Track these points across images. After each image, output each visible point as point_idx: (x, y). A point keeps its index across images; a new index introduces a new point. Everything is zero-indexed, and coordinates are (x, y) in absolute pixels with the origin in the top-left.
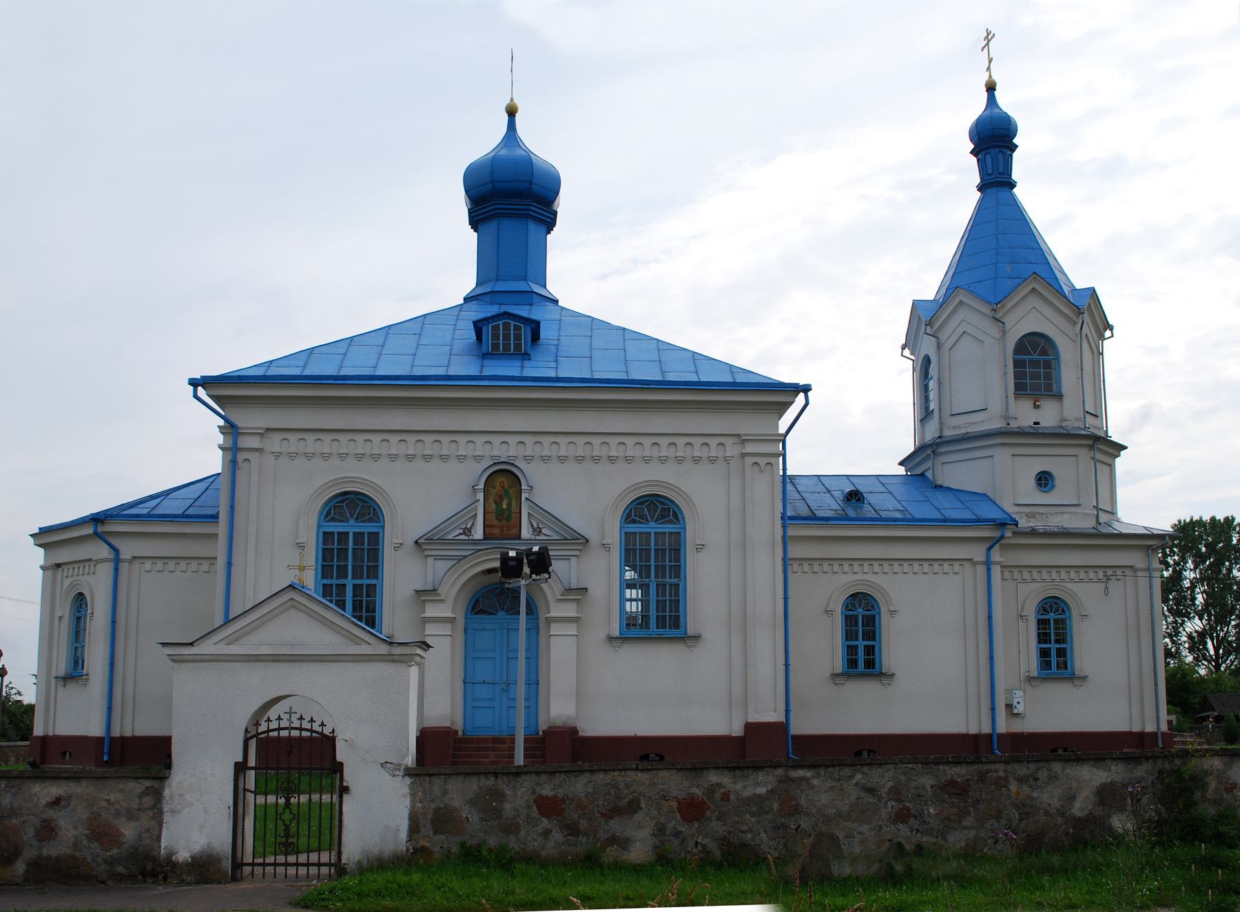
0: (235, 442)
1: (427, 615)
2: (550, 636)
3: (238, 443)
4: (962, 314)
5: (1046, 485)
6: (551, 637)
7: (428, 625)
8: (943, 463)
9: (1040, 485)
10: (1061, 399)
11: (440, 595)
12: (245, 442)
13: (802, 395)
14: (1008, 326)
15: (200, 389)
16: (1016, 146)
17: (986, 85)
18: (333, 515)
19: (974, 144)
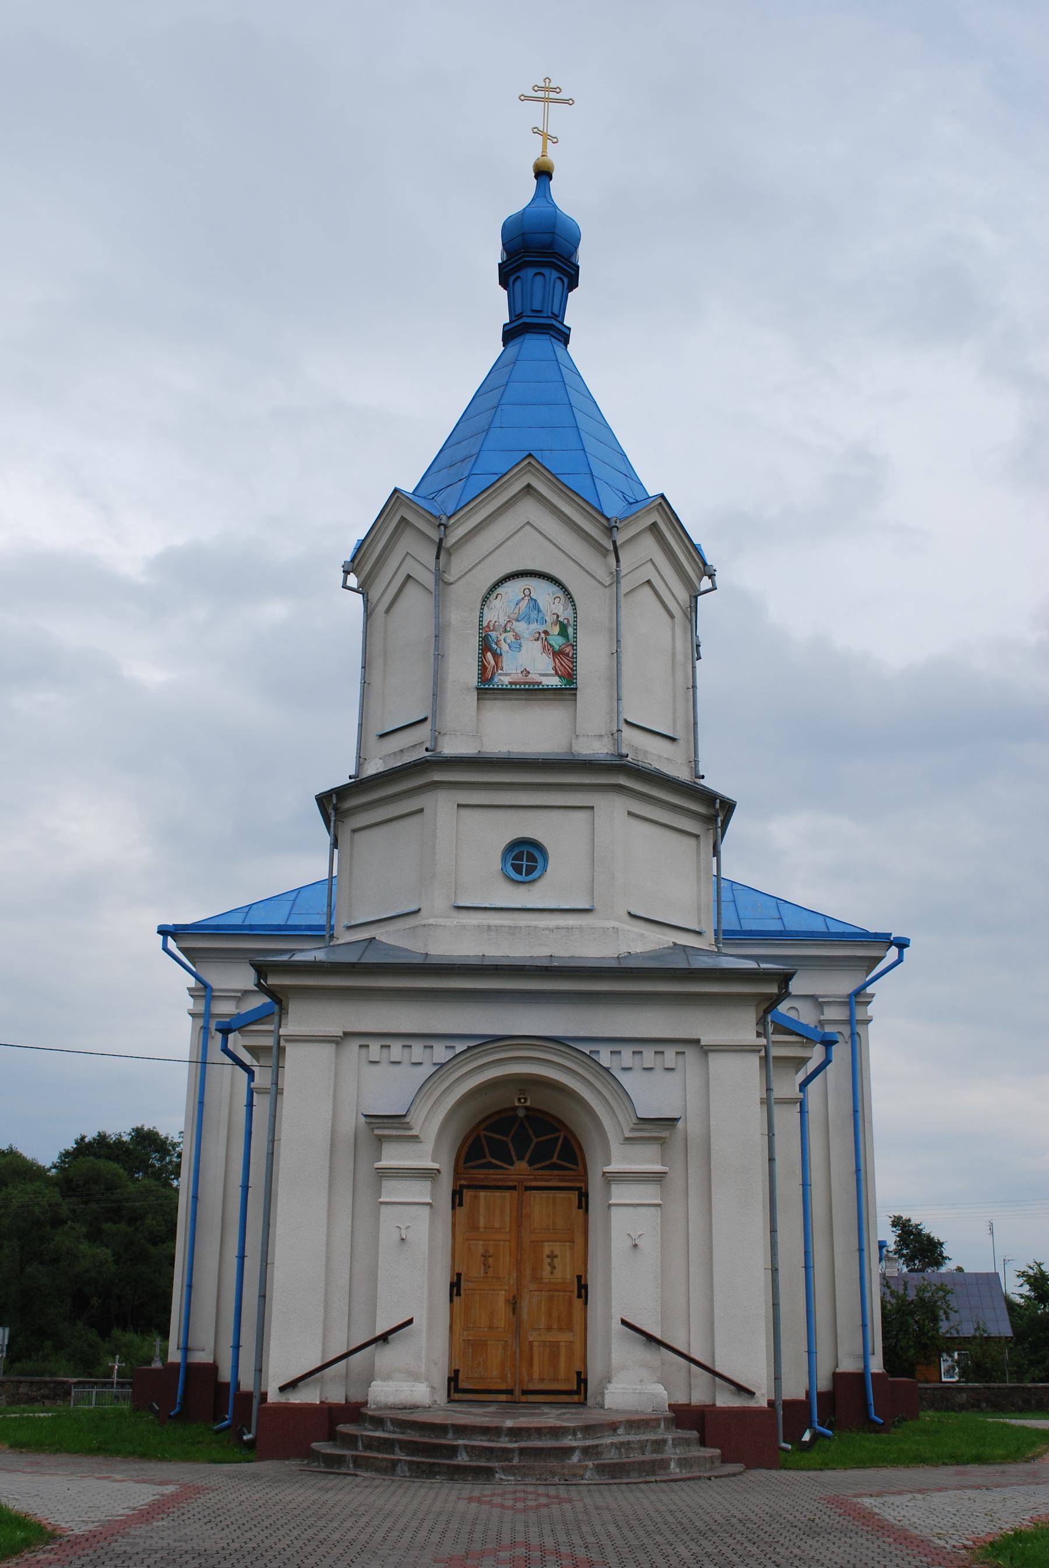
0: (208, 1007)
1: (384, 1163)
2: (610, 1206)
3: (212, 1009)
5: (530, 870)
6: (613, 1208)
7: (387, 1184)
8: (354, 831)
9: (518, 869)
11: (410, 1129)
13: (894, 950)
14: (624, 567)
15: (170, 941)
18: (535, 1140)
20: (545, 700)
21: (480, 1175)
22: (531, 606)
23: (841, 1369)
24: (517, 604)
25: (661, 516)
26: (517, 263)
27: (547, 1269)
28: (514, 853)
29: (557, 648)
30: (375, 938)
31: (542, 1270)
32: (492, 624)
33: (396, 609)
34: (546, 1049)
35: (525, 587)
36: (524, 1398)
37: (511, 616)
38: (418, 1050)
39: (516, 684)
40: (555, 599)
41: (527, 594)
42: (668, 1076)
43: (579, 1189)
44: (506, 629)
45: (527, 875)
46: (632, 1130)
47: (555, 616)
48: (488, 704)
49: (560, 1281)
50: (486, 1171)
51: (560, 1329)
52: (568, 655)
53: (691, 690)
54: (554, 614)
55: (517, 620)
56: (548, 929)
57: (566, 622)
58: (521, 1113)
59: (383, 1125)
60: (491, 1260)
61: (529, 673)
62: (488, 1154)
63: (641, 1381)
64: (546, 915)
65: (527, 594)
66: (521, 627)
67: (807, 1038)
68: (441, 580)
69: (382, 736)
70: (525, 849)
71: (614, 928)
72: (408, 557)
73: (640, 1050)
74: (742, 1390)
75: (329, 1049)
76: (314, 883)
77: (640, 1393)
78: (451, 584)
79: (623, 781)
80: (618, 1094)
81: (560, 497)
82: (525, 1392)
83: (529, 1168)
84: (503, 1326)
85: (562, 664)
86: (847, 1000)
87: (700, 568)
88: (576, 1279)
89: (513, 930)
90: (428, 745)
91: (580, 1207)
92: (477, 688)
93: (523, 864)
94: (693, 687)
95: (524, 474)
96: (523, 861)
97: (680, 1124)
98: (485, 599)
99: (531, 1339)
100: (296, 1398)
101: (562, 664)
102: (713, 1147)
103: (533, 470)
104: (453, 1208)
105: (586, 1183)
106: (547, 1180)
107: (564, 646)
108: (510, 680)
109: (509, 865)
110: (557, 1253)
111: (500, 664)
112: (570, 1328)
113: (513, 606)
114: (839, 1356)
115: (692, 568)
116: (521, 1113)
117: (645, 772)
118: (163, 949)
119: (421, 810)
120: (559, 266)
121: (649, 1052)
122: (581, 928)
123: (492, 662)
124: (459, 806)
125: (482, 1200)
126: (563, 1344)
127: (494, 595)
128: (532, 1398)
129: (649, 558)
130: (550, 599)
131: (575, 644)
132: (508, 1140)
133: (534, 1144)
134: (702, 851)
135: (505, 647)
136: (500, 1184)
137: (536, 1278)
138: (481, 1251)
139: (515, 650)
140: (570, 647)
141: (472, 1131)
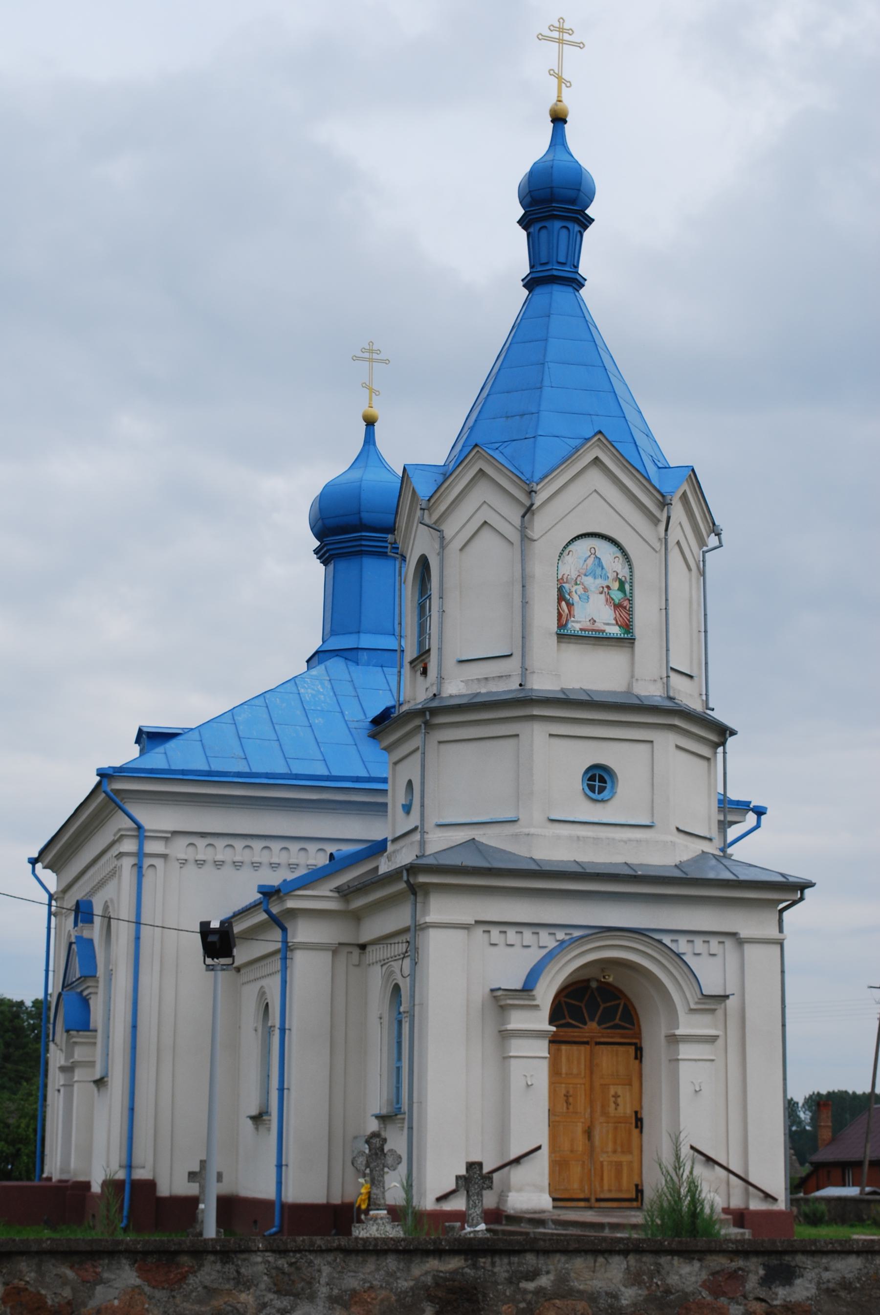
0: (141, 846)
5: (602, 790)
8: (440, 742)
9: (592, 788)
10: (633, 643)
11: (534, 1000)
12: (151, 847)
16: (591, 220)
17: (551, 115)
18: (602, 1006)
19: (524, 208)
20: (608, 645)
22: (596, 564)
24: (585, 561)
25: (690, 487)
27: (613, 1106)
29: (617, 601)
30: (474, 839)
31: (609, 1107)
32: (565, 577)
33: (468, 549)
34: (647, 944)
35: (591, 546)
37: (581, 571)
38: (528, 935)
39: (585, 630)
40: (615, 558)
41: (593, 552)
43: (635, 1044)
44: (576, 582)
47: (615, 574)
48: (564, 646)
49: (622, 1115)
51: (623, 1152)
52: (625, 608)
53: (664, 611)
54: (614, 572)
55: (585, 575)
56: (621, 841)
57: (623, 579)
61: (595, 621)
62: (567, 1017)
64: (618, 829)
65: (593, 552)
66: (588, 581)
68: (525, 538)
71: (671, 842)
72: (485, 506)
74: (768, 1197)
76: (208, 722)
78: (535, 540)
79: (677, 722)
80: (687, 976)
81: (622, 470)
82: (598, 1200)
85: (621, 616)
87: (710, 527)
88: (634, 1114)
91: (636, 1058)
92: (558, 634)
93: (595, 785)
94: (666, 609)
96: (595, 781)
97: (731, 1003)
99: (601, 1159)
101: (621, 616)
105: (640, 1038)
106: (612, 1037)
107: (622, 600)
110: (620, 1093)
111: (572, 612)
112: (630, 1152)
113: (582, 562)
115: (704, 526)
116: (594, 985)
117: (694, 715)
125: (563, 1052)
126: (625, 1163)
127: (567, 551)
131: (631, 599)
132: (582, 1005)
135: (576, 598)
137: (604, 1113)
138: (563, 1092)
140: (627, 601)
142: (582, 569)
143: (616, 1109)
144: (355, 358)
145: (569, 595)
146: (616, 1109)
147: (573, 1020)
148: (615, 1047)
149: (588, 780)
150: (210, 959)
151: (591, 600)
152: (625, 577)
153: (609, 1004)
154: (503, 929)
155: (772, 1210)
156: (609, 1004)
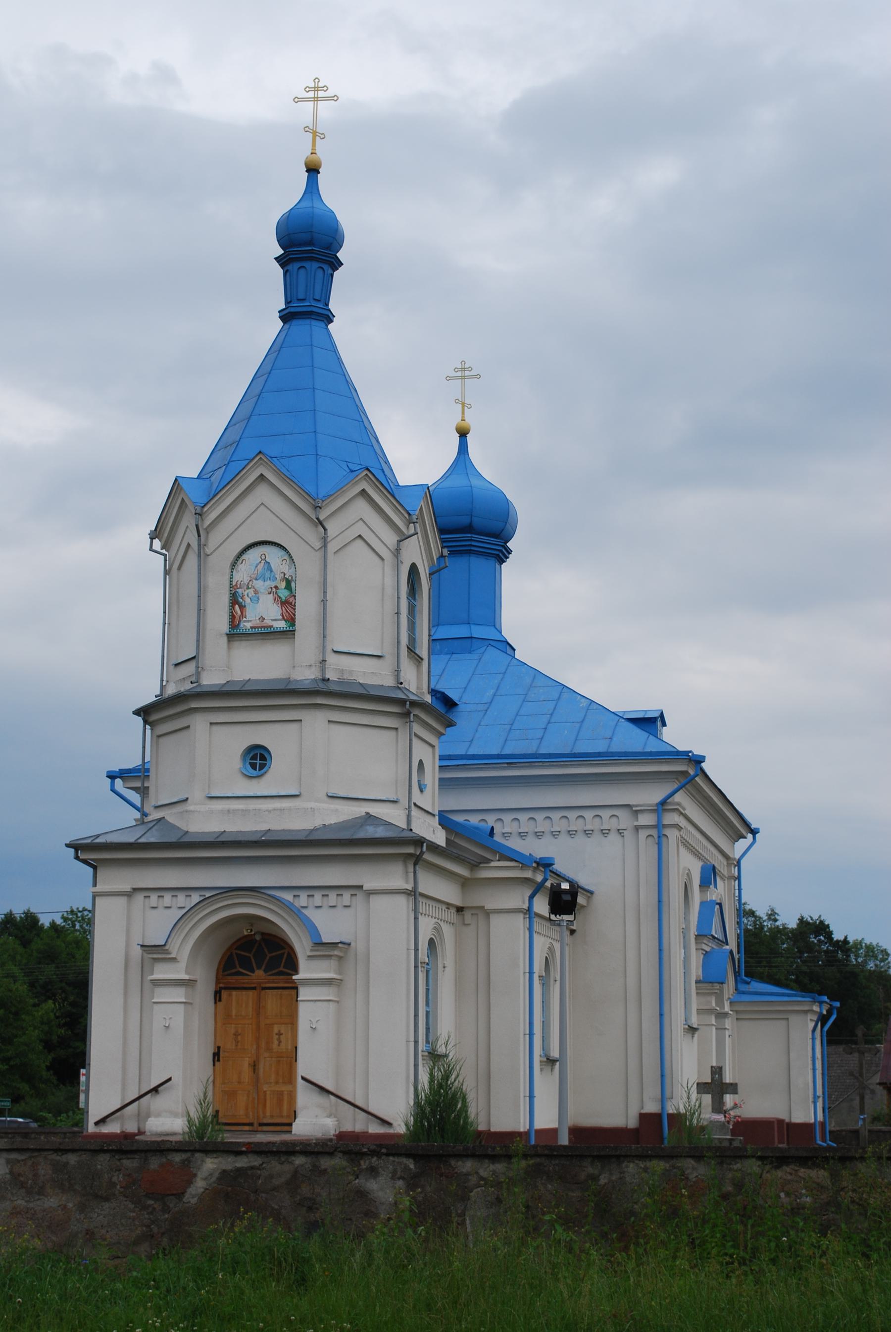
0: (659, 819)
4: (263, 493)
5: (262, 767)
7: (158, 990)
9: (253, 766)
11: (170, 953)
14: (331, 533)
15: (118, 781)
18: (269, 956)
21: (232, 980)
23: (645, 1111)
26: (285, 259)
27: (276, 1042)
28: (251, 755)
29: (284, 599)
31: (273, 1043)
32: (239, 583)
33: (184, 567)
35: (262, 553)
36: (260, 1128)
38: (168, 899)
42: (347, 910)
45: (259, 770)
46: (311, 950)
47: (283, 575)
48: (236, 644)
49: (284, 1050)
50: (236, 977)
55: (256, 579)
57: (290, 578)
58: (258, 938)
59: (152, 952)
60: (239, 1037)
61: (264, 619)
62: (238, 967)
63: (317, 1116)
66: (259, 584)
67: (522, 864)
69: (177, 665)
70: (259, 752)
73: (326, 893)
75: (123, 900)
77: (314, 1124)
82: (261, 1125)
83: (264, 975)
84: (247, 1080)
85: (287, 611)
86: (656, 808)
89: (245, 812)
90: (193, 679)
92: (227, 634)
95: (258, 467)
96: (260, 760)
98: (234, 565)
99: (265, 1090)
100: (106, 1129)
101: (287, 611)
102: (371, 959)
103: (264, 463)
104: (215, 1003)
108: (252, 626)
109: (248, 763)
110: (282, 1032)
111: (244, 614)
113: (253, 568)
114: (644, 1100)
118: (111, 790)
119: (188, 727)
120: (316, 258)
121: (332, 895)
122: (290, 809)
123: (239, 612)
124: (211, 724)
127: (240, 561)
128: (265, 1128)
129: (359, 518)
130: (279, 561)
132: (251, 956)
133: (268, 958)
134: (399, 741)
135: (248, 600)
136: (245, 986)
137: (269, 1049)
138: (233, 1031)
139: (255, 602)
141: (228, 950)
142: (253, 574)
143: (279, 1045)
144: (448, 378)
145: (242, 599)
146: (279, 1045)
147: (244, 969)
148: (280, 991)
149: (250, 759)
150: (554, 915)
151: (261, 601)
152: (291, 576)
153: (274, 954)
154: (189, 893)
155: (389, 1133)
156: (274, 954)
